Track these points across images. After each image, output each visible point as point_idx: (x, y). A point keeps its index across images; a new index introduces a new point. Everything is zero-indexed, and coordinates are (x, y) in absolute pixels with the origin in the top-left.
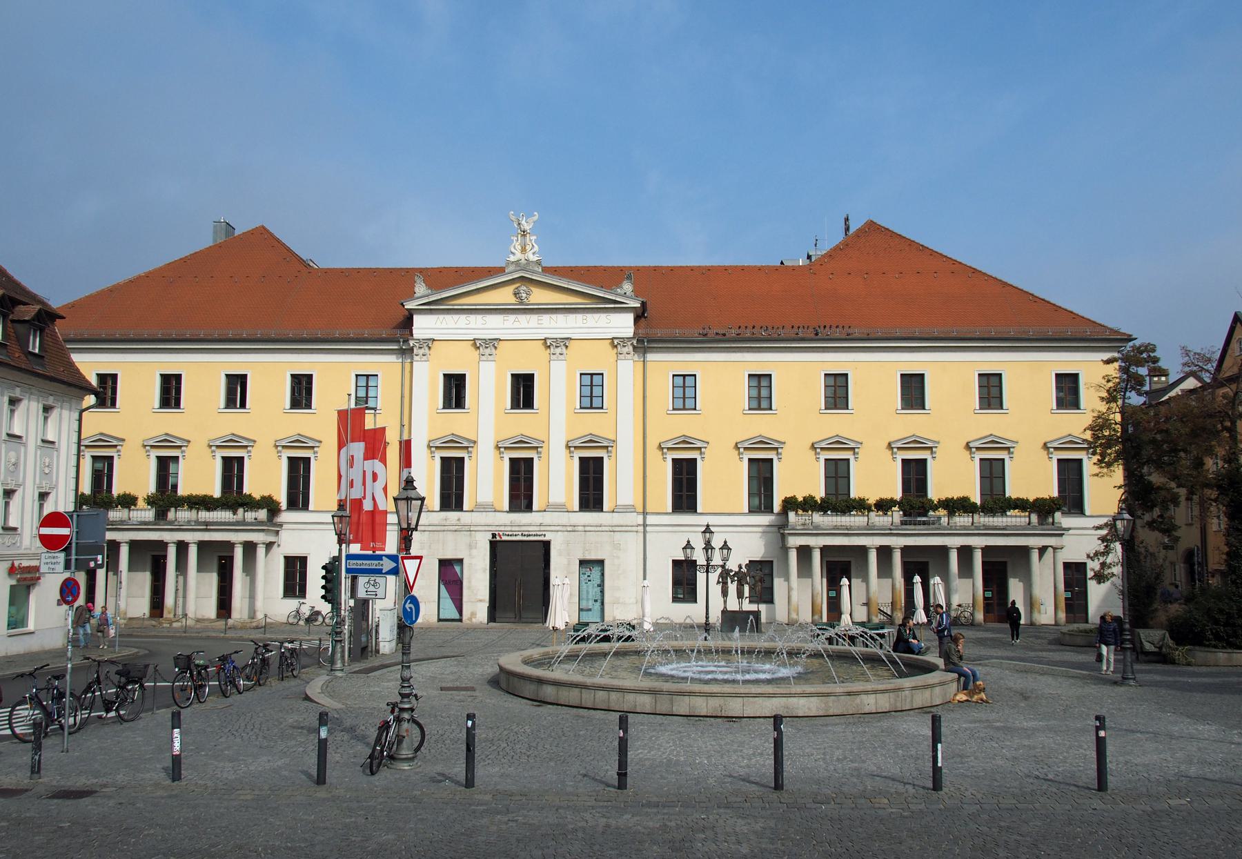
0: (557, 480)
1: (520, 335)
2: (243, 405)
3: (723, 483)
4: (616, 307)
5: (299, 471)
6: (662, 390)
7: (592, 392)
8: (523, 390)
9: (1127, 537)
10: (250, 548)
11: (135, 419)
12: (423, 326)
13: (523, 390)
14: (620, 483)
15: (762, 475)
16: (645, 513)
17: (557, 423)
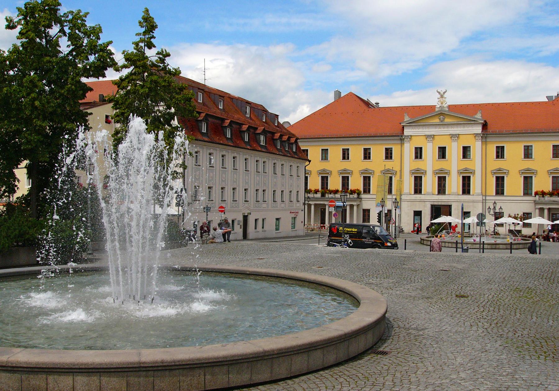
0: (454, 184)
1: (442, 134)
2: (348, 158)
3: (513, 184)
4: (473, 122)
5: (367, 180)
6: (492, 150)
7: (466, 151)
8: (442, 152)
9: (258, 137)
10: (352, 206)
11: (315, 163)
12: (407, 132)
13: (442, 152)
14: (476, 184)
15: (528, 181)
16: (486, 196)
17: (454, 163)
